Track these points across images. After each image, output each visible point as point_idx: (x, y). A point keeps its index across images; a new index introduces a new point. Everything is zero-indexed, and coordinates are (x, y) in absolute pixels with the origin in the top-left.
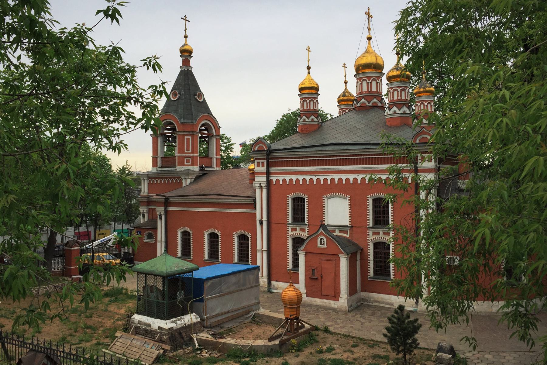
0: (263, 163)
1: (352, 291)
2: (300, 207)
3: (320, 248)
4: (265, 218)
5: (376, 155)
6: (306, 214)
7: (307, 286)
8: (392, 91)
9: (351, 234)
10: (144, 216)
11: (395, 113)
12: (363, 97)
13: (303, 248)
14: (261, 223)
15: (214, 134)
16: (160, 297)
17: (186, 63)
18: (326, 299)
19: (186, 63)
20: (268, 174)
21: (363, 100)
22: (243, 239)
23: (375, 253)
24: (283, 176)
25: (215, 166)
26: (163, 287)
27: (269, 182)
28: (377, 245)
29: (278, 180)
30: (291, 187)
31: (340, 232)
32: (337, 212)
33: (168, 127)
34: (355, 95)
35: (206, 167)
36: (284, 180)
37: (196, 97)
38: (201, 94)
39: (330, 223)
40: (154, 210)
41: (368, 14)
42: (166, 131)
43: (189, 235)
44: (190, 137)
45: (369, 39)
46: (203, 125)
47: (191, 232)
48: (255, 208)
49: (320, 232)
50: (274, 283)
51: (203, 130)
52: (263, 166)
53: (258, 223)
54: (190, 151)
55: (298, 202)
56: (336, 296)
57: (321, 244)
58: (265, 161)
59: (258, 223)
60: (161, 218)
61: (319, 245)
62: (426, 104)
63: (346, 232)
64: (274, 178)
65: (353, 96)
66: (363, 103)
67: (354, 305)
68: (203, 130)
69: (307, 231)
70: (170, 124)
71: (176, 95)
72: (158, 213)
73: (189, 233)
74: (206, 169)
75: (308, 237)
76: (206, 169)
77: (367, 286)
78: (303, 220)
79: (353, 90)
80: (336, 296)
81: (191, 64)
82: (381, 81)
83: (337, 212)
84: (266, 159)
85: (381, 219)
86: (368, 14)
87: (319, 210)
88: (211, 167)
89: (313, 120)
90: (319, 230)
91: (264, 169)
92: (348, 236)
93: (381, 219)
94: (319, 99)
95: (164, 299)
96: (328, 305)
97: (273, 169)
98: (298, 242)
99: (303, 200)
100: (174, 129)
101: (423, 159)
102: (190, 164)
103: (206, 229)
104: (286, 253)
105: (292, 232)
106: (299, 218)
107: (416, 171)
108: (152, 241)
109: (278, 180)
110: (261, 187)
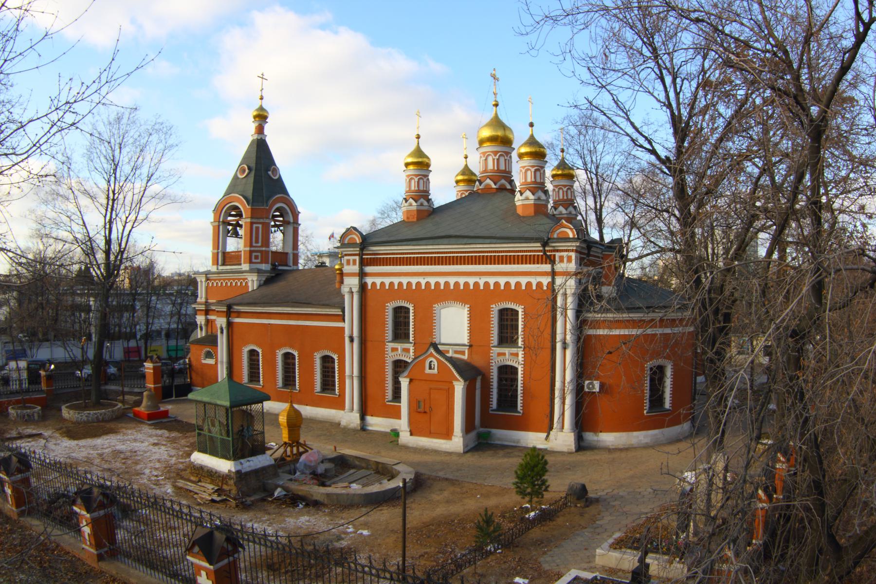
0: (354, 261)
1: (469, 426)
2: (402, 319)
3: (429, 374)
4: (356, 334)
5: (504, 252)
6: (411, 330)
7: (411, 422)
8: (524, 171)
9: (470, 354)
10: (201, 329)
11: (527, 199)
12: (488, 177)
13: (406, 374)
14: (352, 340)
15: (292, 221)
16: (224, 432)
17: (260, 130)
18: (437, 438)
19: (260, 130)
20: (362, 275)
21: (488, 181)
22: (327, 361)
23: (500, 379)
24: (380, 277)
25: (291, 264)
26: (227, 420)
27: (363, 287)
28: (503, 312)
29: (374, 284)
30: (393, 292)
31: (456, 352)
32: (453, 326)
33: (233, 213)
34: (477, 173)
35: (280, 265)
36: (382, 284)
37: (270, 173)
38: (276, 170)
39: (443, 341)
40: (213, 321)
41: (494, 77)
42: (230, 218)
43: (258, 355)
44: (260, 226)
45: (496, 105)
46: (277, 210)
47: (260, 351)
48: (344, 321)
49: (429, 353)
50: (369, 419)
51: (277, 216)
52: (354, 263)
53: (347, 340)
54: (260, 244)
55: (400, 314)
56: (448, 434)
57: (430, 368)
58: (357, 258)
59: (347, 340)
60: (222, 332)
61: (428, 371)
62: (565, 189)
63: (463, 353)
64: (369, 281)
65: (475, 175)
66: (488, 185)
67: (472, 445)
68: (277, 216)
69: (412, 351)
70: (236, 208)
71: (244, 171)
72: (219, 326)
73: (293, 356)
74: (280, 268)
75: (414, 359)
76: (280, 268)
77: (489, 421)
78: (407, 336)
79: (476, 167)
80: (448, 434)
81: (266, 132)
82: (511, 157)
83: (453, 326)
84: (359, 255)
85: (507, 337)
86: (494, 77)
87: (428, 322)
88: (287, 265)
89: (422, 205)
90: (427, 351)
91: (356, 268)
92: (466, 357)
93: (507, 337)
94: (431, 177)
95: (228, 436)
96: (437, 445)
97: (368, 269)
98: (399, 366)
99: (407, 310)
100: (240, 215)
101: (561, 259)
102: (259, 261)
103: (317, 350)
104: (384, 381)
105: (395, 351)
106: (401, 334)
107: (553, 274)
108: (211, 361)
109: (374, 284)
110: (352, 292)
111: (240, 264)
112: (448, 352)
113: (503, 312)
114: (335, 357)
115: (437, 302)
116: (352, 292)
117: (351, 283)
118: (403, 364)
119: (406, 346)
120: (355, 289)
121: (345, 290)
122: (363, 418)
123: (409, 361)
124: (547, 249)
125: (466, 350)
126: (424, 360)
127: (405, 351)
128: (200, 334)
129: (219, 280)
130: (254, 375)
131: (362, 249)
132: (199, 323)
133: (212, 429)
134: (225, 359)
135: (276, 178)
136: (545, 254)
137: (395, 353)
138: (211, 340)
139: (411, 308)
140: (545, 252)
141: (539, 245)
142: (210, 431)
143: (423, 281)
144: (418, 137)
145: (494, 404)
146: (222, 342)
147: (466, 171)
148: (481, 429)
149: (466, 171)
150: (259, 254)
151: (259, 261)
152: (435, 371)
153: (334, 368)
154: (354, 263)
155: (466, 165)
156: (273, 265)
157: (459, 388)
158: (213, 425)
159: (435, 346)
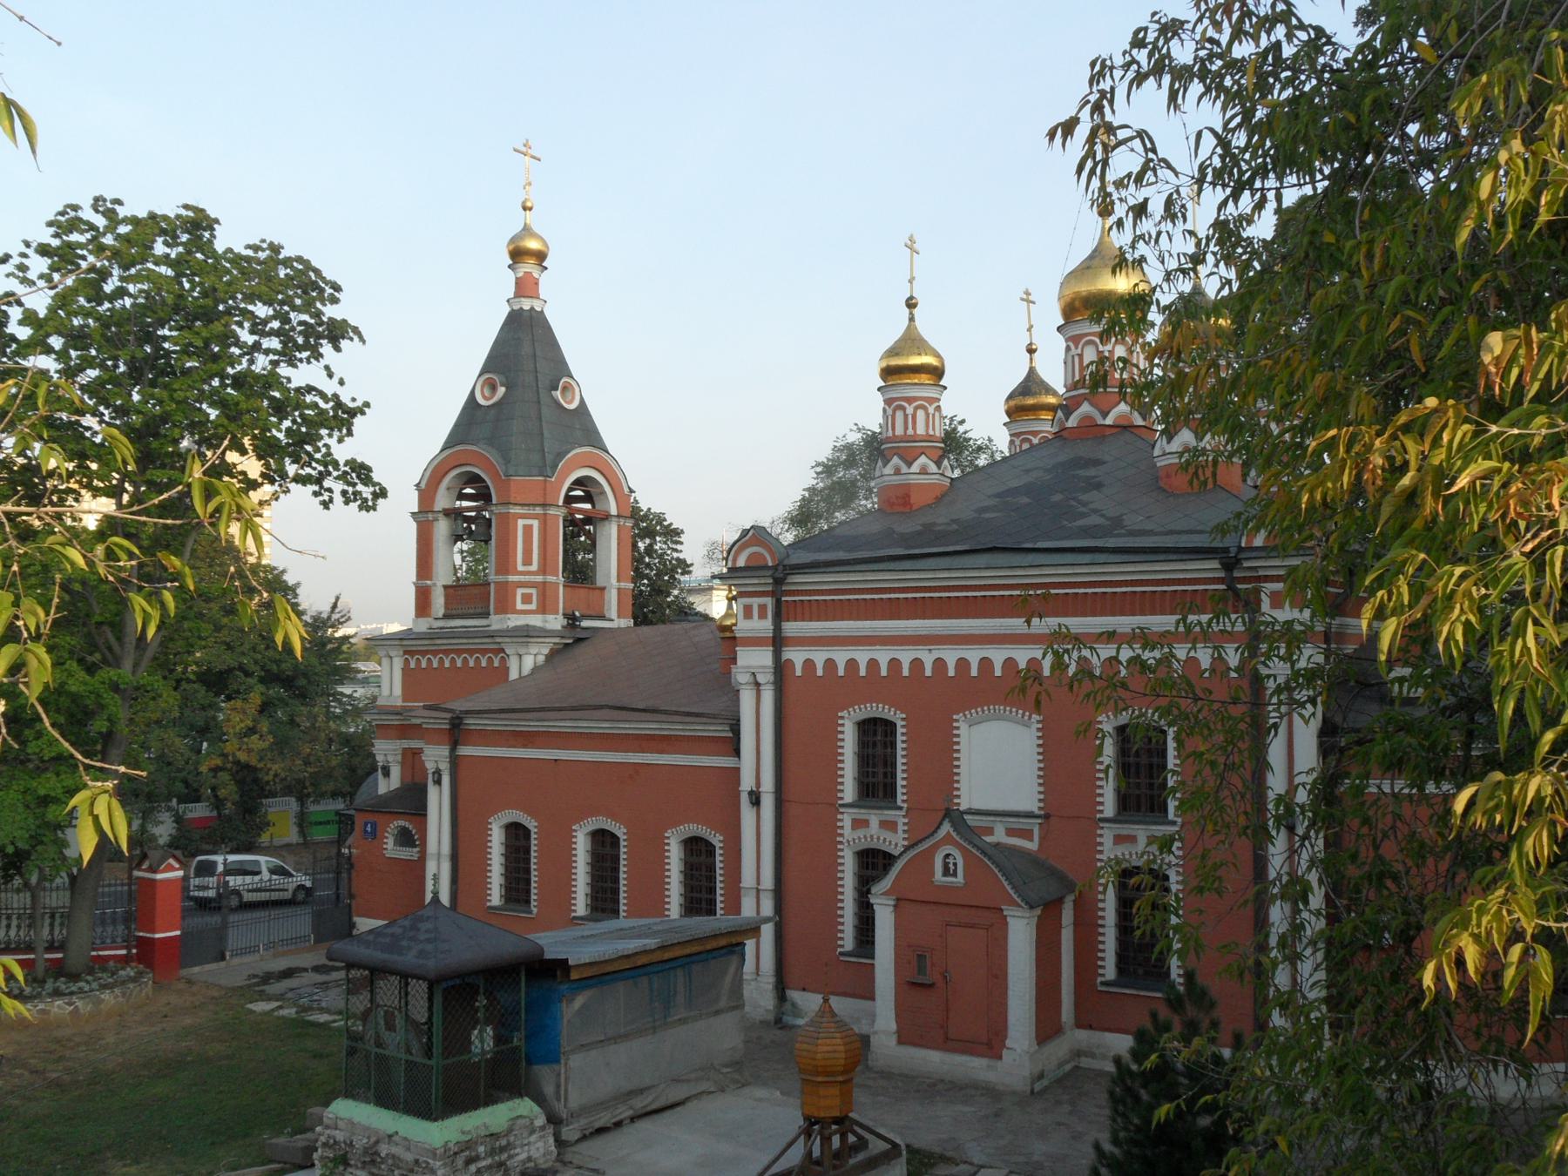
0: (762, 608)
7: (902, 1010)
10: (387, 773)
19: (525, 287)
22: (697, 848)
25: (614, 615)
27: (781, 670)
28: (525, 527)
29: (809, 664)
30: (855, 685)
31: (1011, 832)
33: (468, 491)
35: (584, 617)
37: (558, 394)
44: (535, 523)
46: (579, 483)
48: (737, 752)
52: (762, 615)
54: (534, 567)
55: (875, 734)
57: (946, 872)
58: (769, 602)
59: (744, 798)
60: (438, 782)
63: (1027, 834)
74: (585, 623)
76: (585, 623)
78: (890, 791)
83: (998, 764)
84: (772, 594)
88: (602, 617)
92: (1032, 846)
93: (1142, 794)
97: (791, 628)
98: (873, 863)
102: (533, 606)
106: (876, 786)
111: (486, 615)
112: (990, 831)
113: (525, 527)
114: (717, 840)
115: (962, 710)
116: (757, 684)
117: (754, 660)
118: (880, 861)
119: (890, 814)
120: (766, 678)
121: (741, 677)
122: (781, 996)
123: (896, 853)
124: (1236, 574)
125: (1035, 826)
126: (929, 855)
127: (885, 829)
128: (387, 785)
129: (435, 653)
130: (517, 887)
131: (778, 582)
132: (380, 758)
133: (387, 1036)
134: (446, 848)
135: (573, 406)
136: (1231, 588)
137: (861, 833)
138: (412, 800)
139: (899, 723)
140: (1231, 582)
141: (1215, 564)
142: (379, 1045)
143: (928, 658)
144: (911, 304)
145: (1109, 970)
146: (438, 802)
147: (1031, 384)
148: (1083, 1036)
149: (1031, 384)
150: (533, 591)
151: (533, 606)
152: (960, 878)
153: (712, 868)
154: (762, 615)
155: (1032, 371)
156: (572, 619)
157: (1021, 932)
158: (390, 1027)
159: (954, 816)
